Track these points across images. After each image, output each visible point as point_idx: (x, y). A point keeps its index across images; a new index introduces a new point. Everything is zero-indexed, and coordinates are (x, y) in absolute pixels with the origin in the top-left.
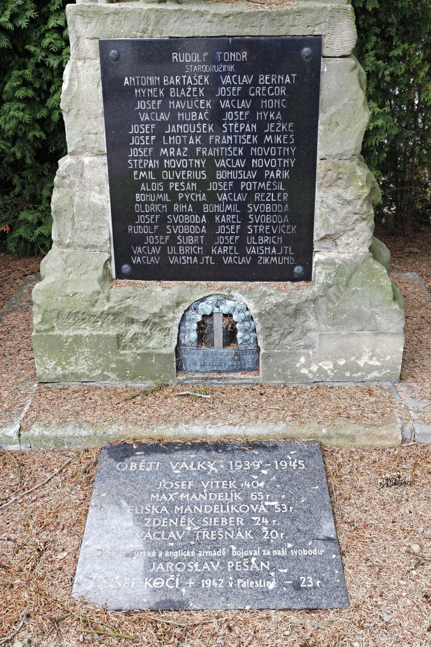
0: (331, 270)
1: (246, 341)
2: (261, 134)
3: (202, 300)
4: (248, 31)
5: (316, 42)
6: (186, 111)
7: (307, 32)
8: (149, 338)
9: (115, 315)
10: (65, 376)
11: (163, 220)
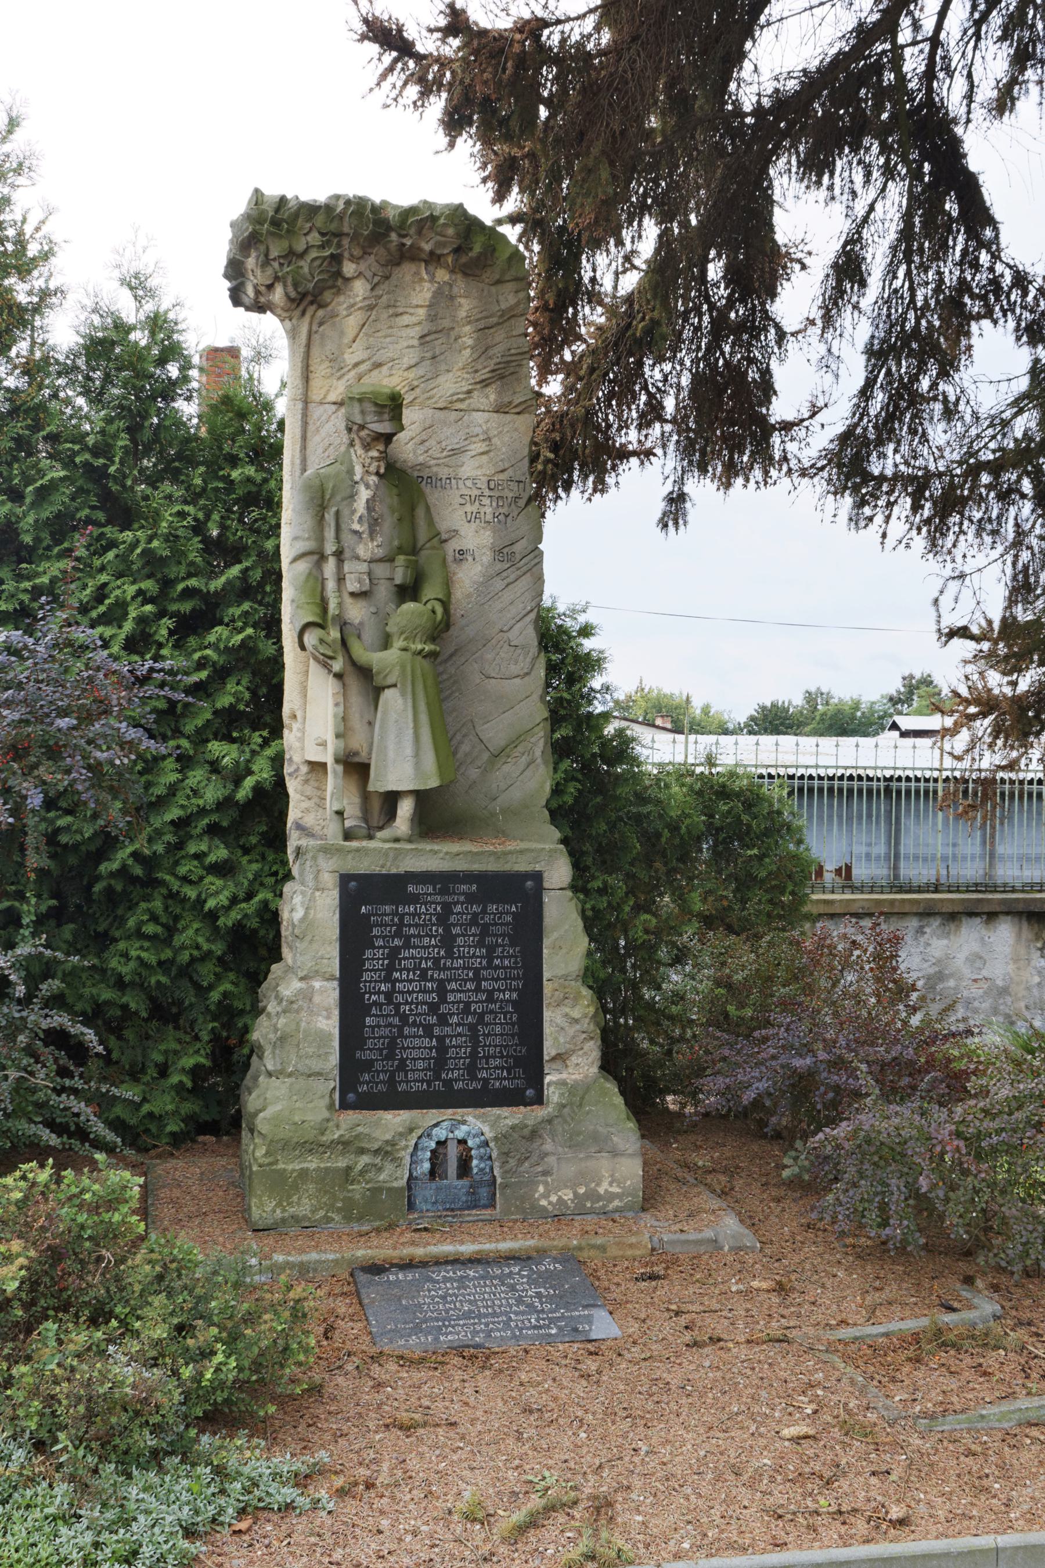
0: (564, 1089)
1: (481, 1170)
2: (490, 958)
3: (436, 1125)
4: (477, 867)
5: (538, 877)
6: (419, 936)
7: (529, 868)
8: (380, 1170)
9: (345, 1145)
10: (283, 1220)
11: (392, 1045)
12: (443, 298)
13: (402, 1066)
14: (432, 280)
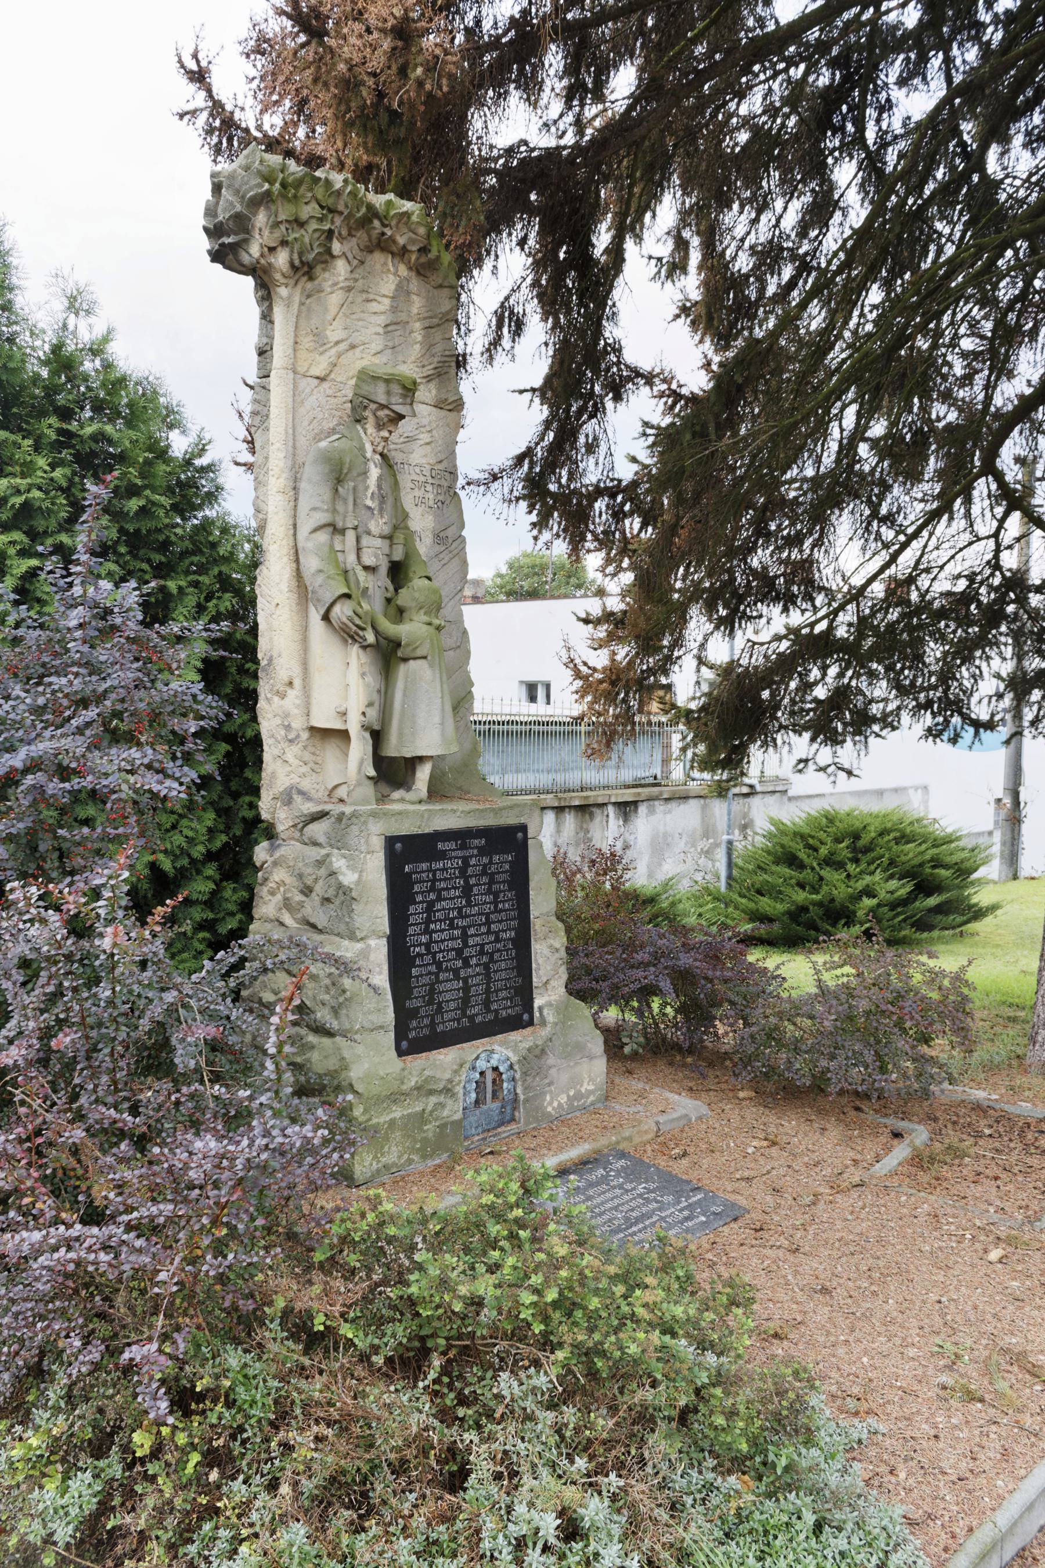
2: (496, 903)
9: (423, 1090)
10: (378, 1171)
11: (432, 991)
12: (401, 292)
13: (440, 1010)
14: (396, 274)
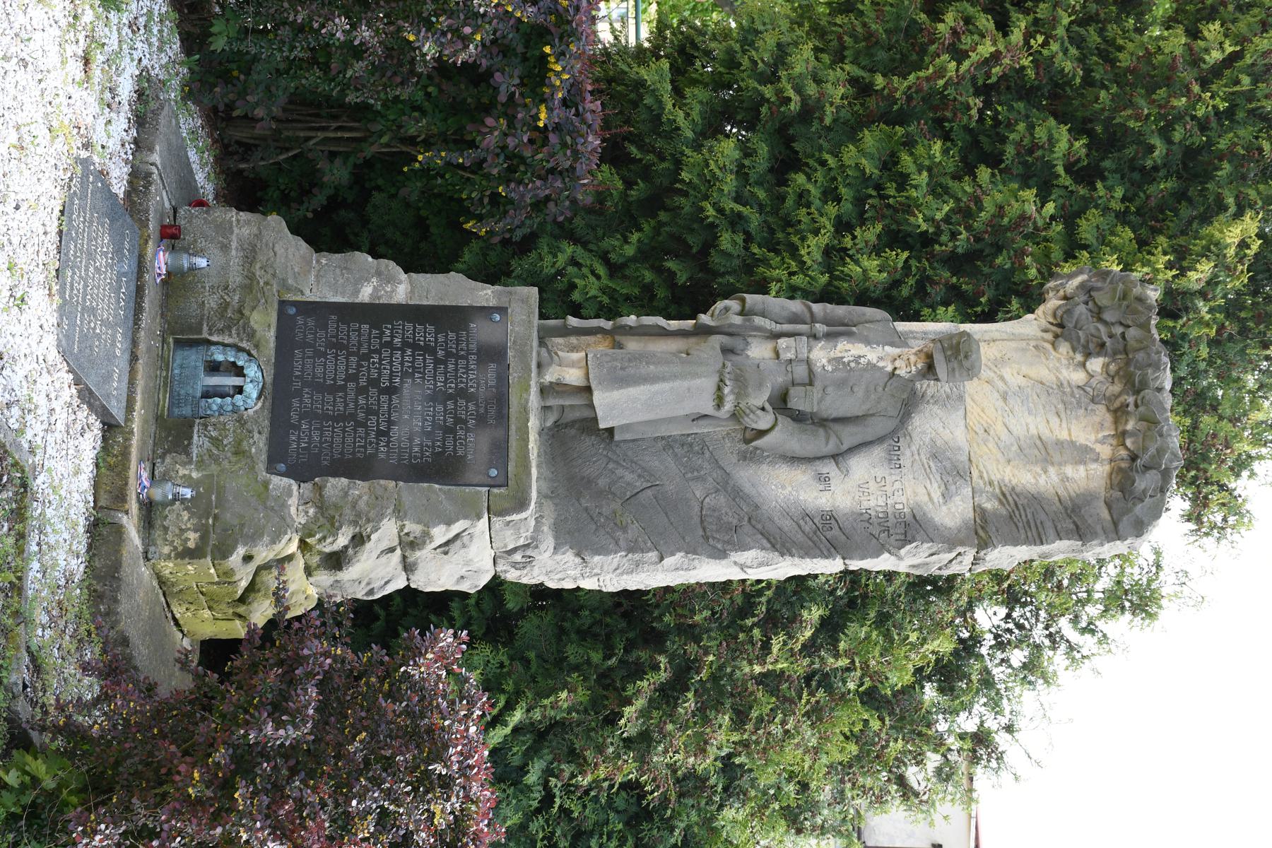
11: (338, 346)
12: (1082, 454)
